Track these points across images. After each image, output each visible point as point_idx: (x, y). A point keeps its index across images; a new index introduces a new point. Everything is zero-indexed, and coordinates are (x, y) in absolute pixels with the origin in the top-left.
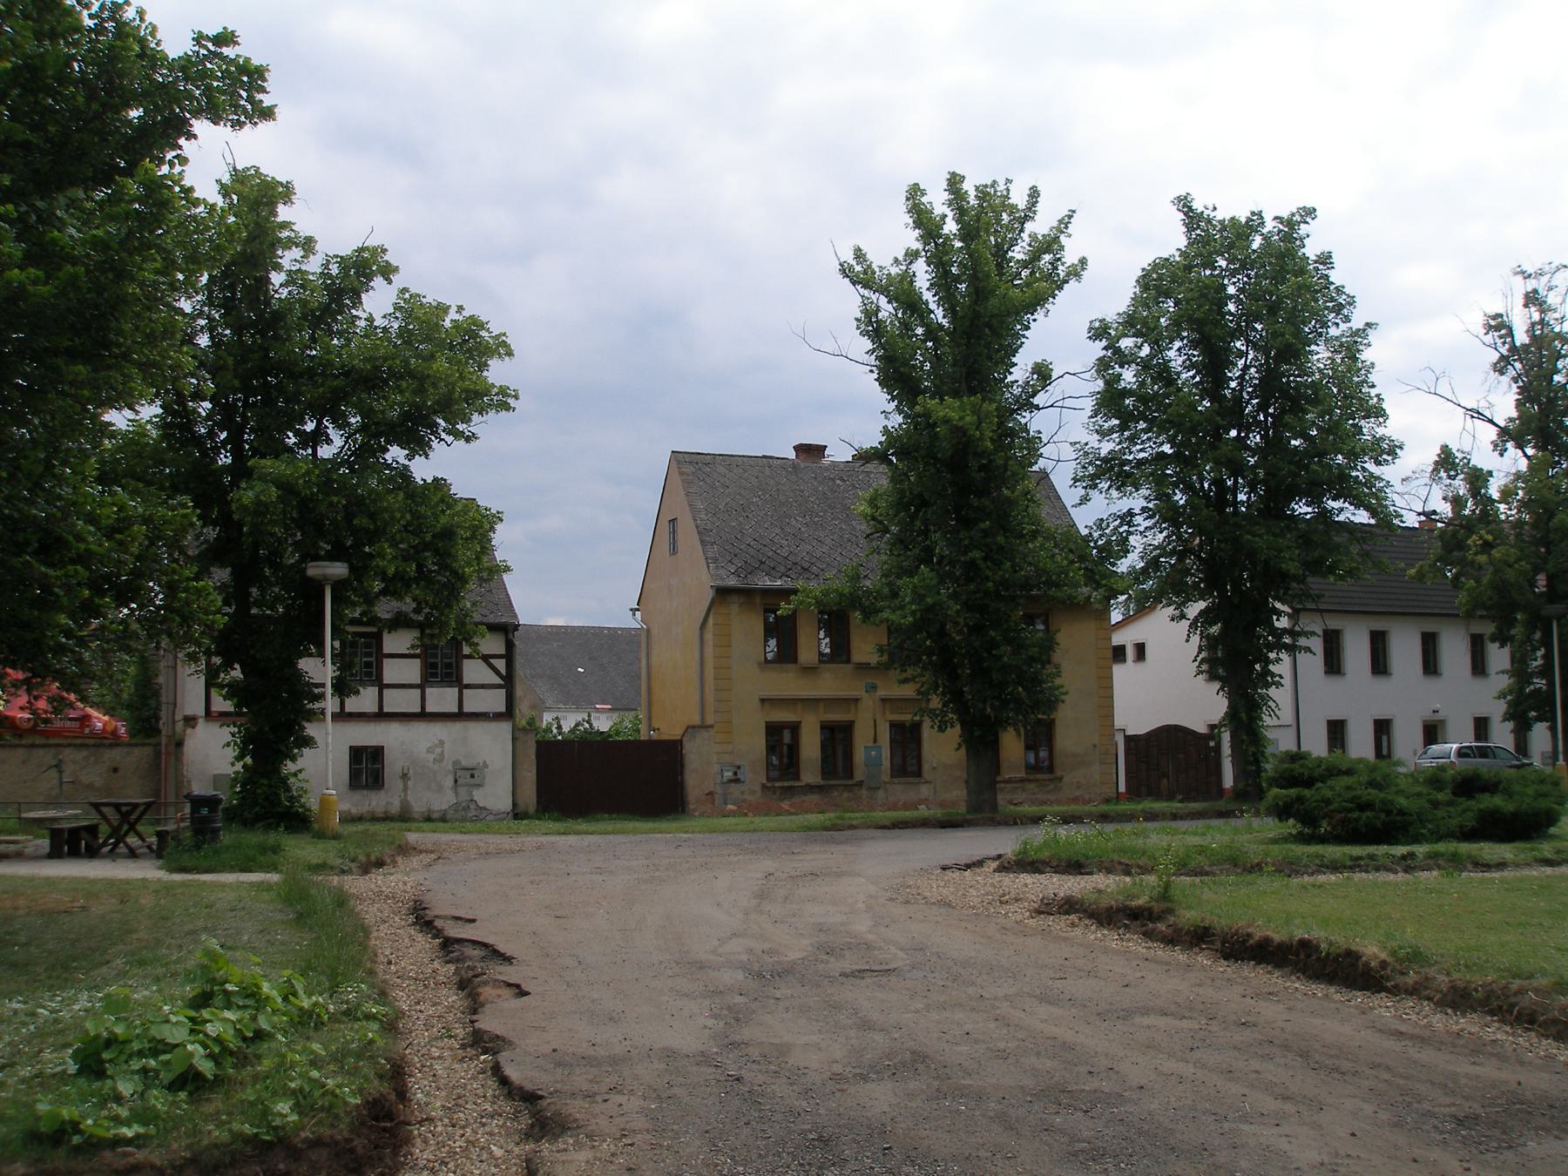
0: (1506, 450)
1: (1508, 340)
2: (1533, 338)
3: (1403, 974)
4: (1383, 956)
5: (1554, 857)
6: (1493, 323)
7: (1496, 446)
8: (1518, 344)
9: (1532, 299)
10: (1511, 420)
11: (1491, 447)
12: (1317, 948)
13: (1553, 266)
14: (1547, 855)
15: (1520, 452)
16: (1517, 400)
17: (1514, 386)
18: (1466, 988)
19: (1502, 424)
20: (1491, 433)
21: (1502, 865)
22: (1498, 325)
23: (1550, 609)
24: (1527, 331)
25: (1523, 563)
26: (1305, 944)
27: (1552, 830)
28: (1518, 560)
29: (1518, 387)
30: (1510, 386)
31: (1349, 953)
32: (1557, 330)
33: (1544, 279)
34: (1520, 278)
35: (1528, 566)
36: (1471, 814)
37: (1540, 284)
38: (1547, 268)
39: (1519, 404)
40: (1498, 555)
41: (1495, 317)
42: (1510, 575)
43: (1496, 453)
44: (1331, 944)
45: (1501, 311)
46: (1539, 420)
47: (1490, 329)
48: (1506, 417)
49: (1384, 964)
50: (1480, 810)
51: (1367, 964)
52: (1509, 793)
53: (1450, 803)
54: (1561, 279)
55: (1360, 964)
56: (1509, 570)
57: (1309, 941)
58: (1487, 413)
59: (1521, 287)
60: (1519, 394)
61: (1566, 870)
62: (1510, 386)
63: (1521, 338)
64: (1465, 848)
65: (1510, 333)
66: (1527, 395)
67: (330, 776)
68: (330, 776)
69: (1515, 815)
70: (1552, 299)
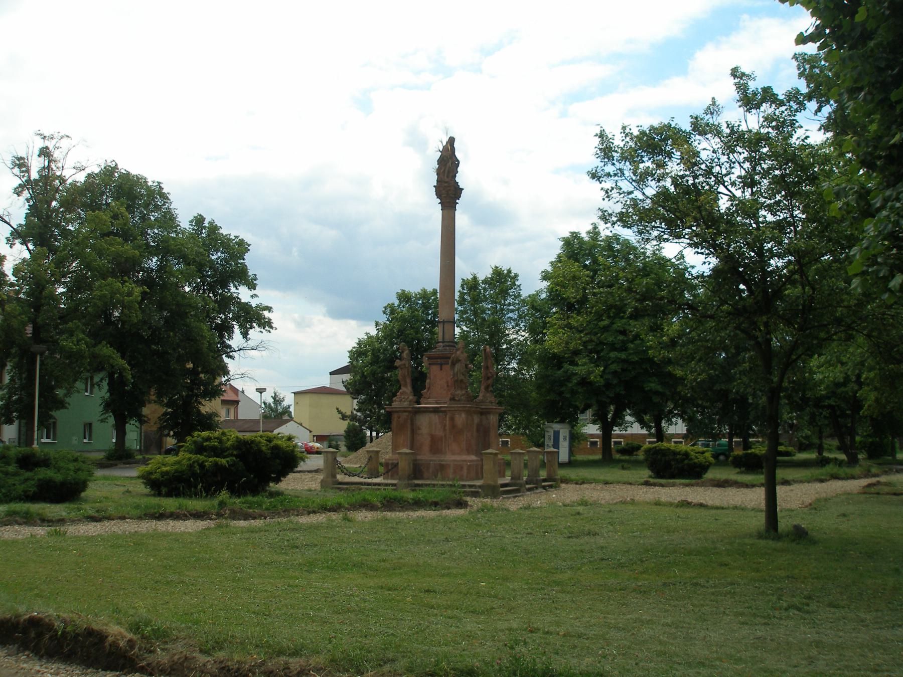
0: (14, 244)
1: (27, 174)
2: (41, 176)
3: (151, 652)
4: (130, 636)
5: (96, 515)
6: (17, 162)
7: (8, 239)
8: (32, 179)
9: (45, 152)
10: (20, 225)
11: (5, 241)
12: (50, 627)
13: (60, 135)
14: (91, 513)
15: (25, 247)
16: (27, 214)
17: (27, 204)
18: (238, 669)
19: (15, 227)
20: (7, 231)
21: (62, 521)
22: (21, 164)
23: (36, 348)
24: (38, 172)
25: (23, 316)
26: (34, 622)
27: (83, 494)
28: (20, 315)
29: (29, 206)
30: (25, 204)
31: (90, 632)
32: (58, 173)
33: (54, 142)
34: (39, 137)
35: (27, 318)
36: (33, 482)
37: (50, 144)
38: (56, 135)
39: (27, 216)
40: (9, 309)
41: (19, 159)
42: (15, 323)
43: (8, 246)
44: (64, 621)
45: (24, 156)
46: (40, 228)
47: (15, 166)
48: (18, 223)
49: (130, 642)
50: (39, 480)
51: (114, 644)
52: (58, 469)
53: (15, 474)
54: (64, 143)
55: (107, 644)
56: (14, 320)
57: (41, 620)
58: (7, 219)
59: (40, 144)
60: (29, 210)
61: (902, 632)
62: (25, 204)
63: (34, 175)
64: (35, 508)
65: (28, 171)
66: (34, 211)
67: (36, 428)
68: (36, 428)
69: (63, 484)
70: (57, 154)
